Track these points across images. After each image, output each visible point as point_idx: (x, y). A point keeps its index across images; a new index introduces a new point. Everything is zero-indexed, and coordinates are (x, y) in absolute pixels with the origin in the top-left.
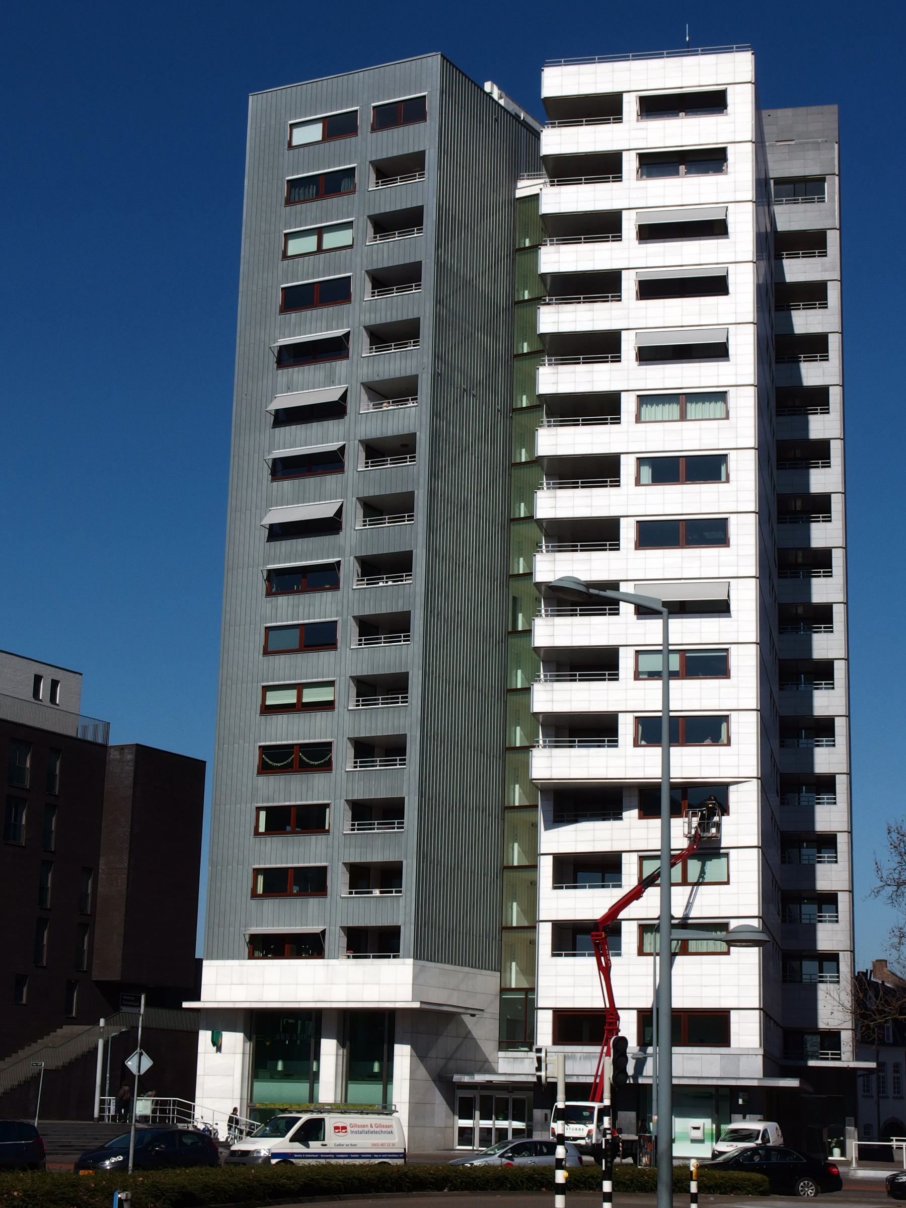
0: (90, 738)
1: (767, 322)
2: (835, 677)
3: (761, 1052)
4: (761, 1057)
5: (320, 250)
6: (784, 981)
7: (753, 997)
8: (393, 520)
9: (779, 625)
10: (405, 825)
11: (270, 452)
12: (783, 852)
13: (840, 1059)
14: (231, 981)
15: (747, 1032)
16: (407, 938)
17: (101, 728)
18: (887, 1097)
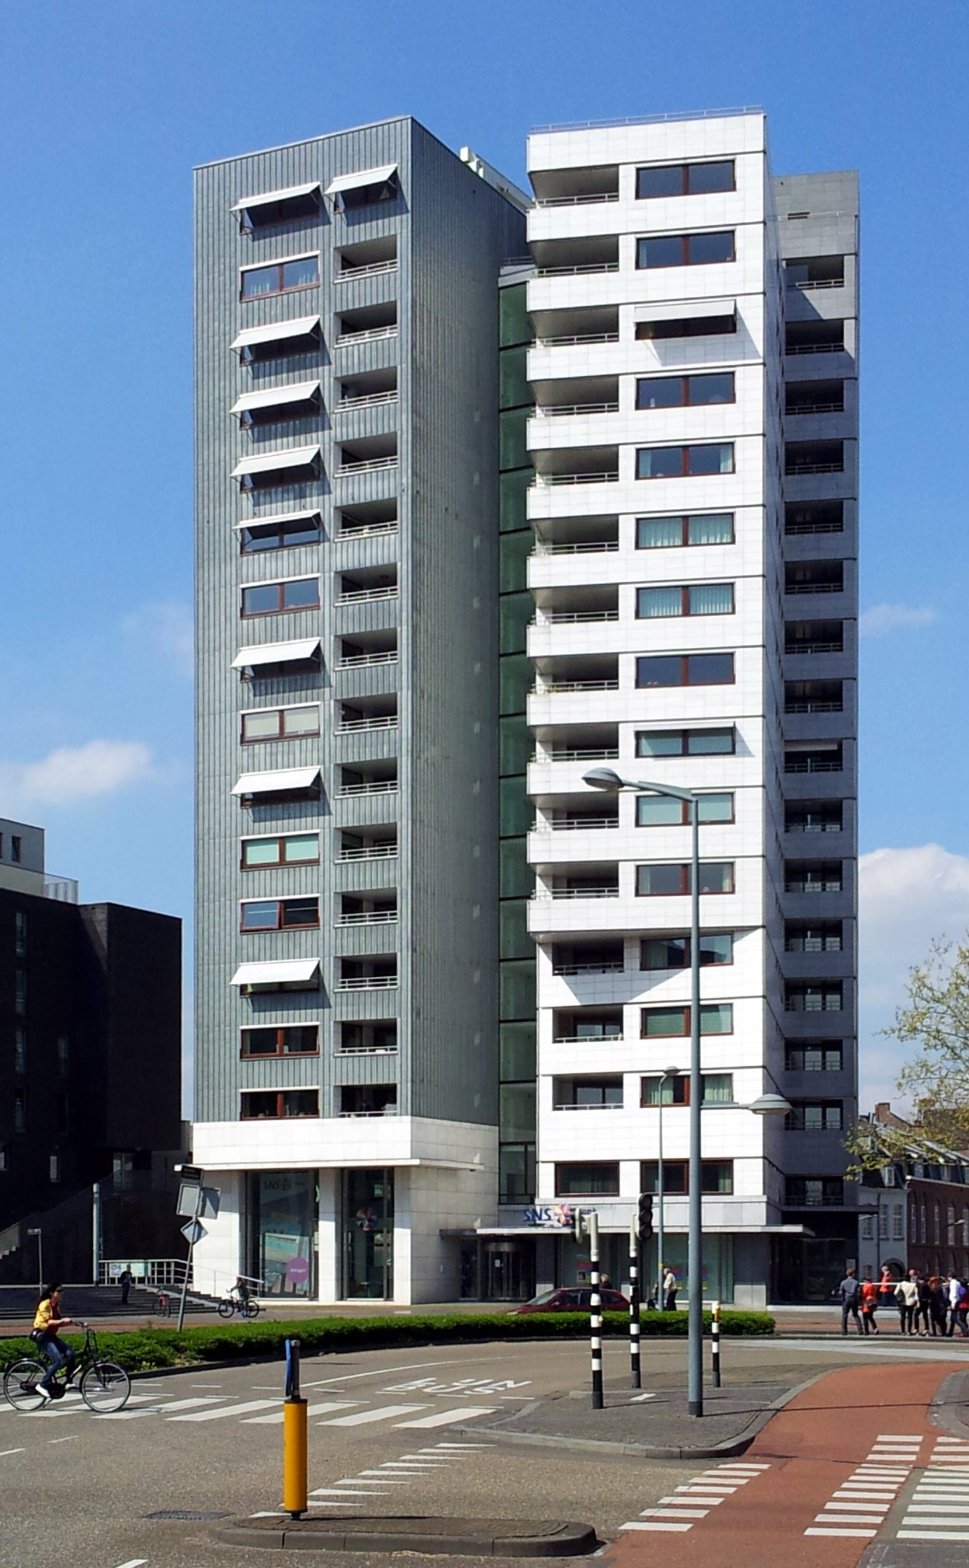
0: (61, 899)
1: (777, 426)
2: (844, 817)
3: (765, 1199)
4: (764, 1205)
5: (283, 862)
6: (787, 1129)
7: (755, 1145)
8: (375, 789)
9: (786, 762)
10: (398, 982)
11: (236, 203)
12: (787, 940)
13: (842, 1204)
14: (223, 1144)
15: (750, 1180)
16: (404, 1093)
17: (70, 886)
18: (888, 1239)
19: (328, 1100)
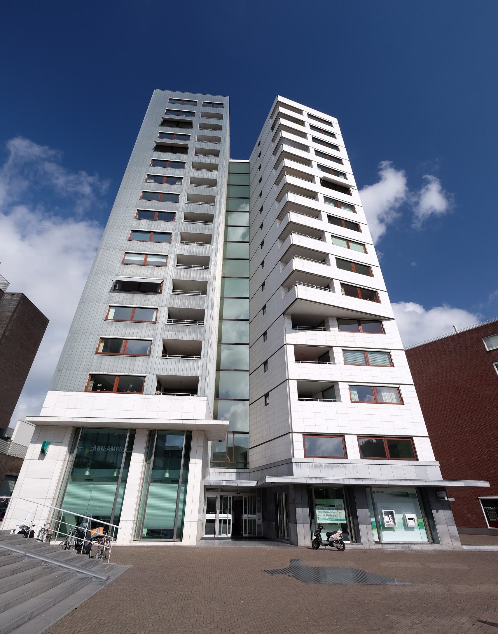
19: (151, 384)
